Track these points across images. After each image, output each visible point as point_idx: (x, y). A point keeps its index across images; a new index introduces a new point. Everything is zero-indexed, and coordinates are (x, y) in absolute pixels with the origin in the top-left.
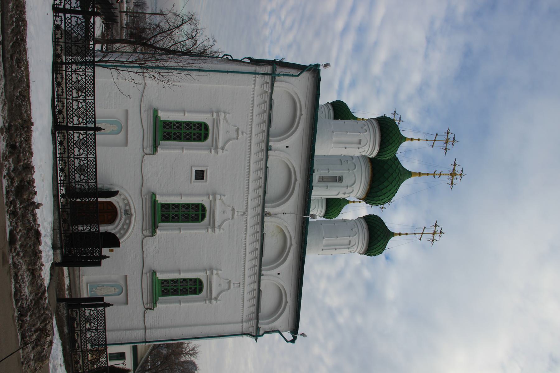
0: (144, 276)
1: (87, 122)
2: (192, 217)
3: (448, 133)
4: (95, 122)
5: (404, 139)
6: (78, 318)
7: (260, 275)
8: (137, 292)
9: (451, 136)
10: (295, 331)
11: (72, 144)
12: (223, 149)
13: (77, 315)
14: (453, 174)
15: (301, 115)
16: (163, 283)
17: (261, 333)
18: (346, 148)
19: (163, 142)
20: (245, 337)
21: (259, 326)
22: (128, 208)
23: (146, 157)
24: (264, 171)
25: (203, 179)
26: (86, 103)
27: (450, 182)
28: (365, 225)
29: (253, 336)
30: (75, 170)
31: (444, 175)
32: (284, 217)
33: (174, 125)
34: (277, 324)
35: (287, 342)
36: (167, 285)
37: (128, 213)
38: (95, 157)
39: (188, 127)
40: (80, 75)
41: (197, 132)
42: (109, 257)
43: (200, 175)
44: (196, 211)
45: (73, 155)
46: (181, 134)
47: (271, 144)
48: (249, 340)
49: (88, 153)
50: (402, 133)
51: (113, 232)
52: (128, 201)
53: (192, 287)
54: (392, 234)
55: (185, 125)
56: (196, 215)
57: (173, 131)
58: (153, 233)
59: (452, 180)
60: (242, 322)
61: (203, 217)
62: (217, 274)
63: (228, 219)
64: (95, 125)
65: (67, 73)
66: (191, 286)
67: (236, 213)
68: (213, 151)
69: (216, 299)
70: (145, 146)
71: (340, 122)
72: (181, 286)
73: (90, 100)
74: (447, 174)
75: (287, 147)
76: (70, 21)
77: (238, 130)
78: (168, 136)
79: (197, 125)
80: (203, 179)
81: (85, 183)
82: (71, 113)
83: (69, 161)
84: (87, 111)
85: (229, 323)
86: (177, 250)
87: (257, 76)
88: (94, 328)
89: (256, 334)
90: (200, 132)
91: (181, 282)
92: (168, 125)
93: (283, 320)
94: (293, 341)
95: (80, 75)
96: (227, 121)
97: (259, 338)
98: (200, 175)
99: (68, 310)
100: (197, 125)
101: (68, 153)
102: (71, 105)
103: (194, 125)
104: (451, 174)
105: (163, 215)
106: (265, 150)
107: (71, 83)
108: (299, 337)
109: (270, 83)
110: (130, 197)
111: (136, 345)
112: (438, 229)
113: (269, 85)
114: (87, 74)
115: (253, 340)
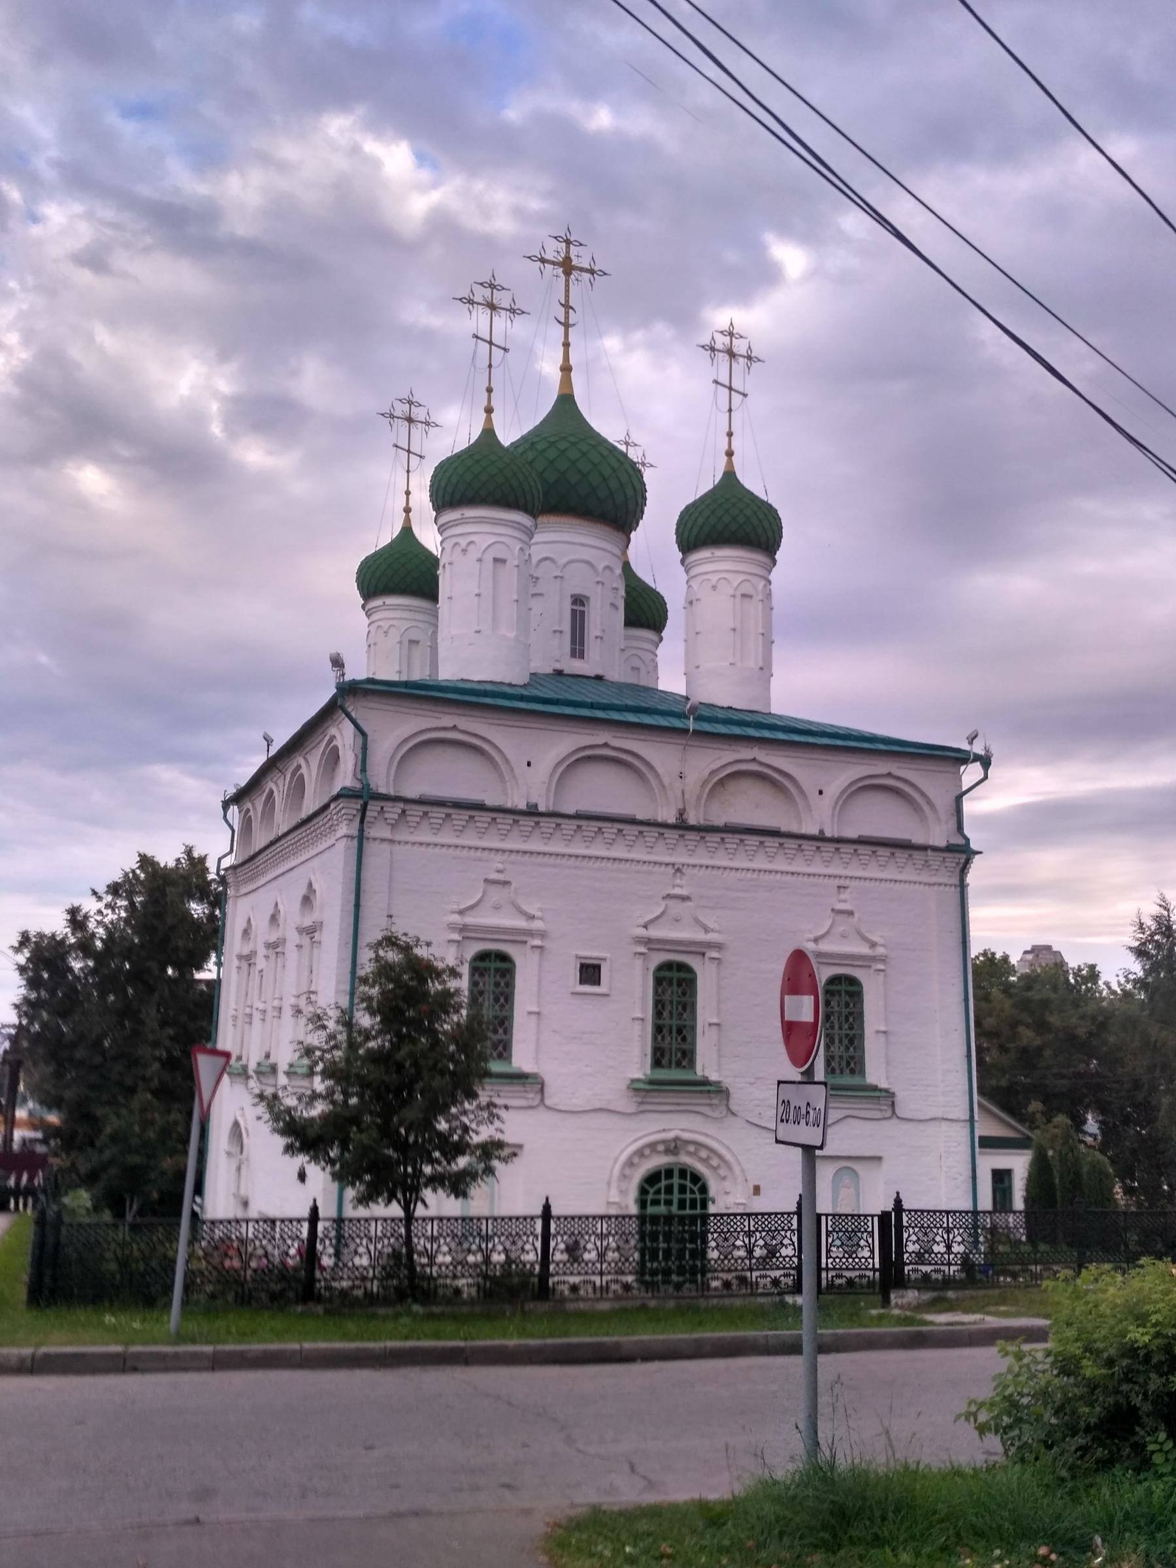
2: (684, 994)
4: (299, 1221)
6: (848, 1274)
10: (960, 758)
13: (841, 1276)
16: (833, 1071)
19: (514, 1059)
20: (970, 879)
21: (942, 843)
22: (661, 1148)
23: (548, 1102)
24: (583, 823)
28: (705, 554)
32: (681, 773)
35: (986, 777)
36: (837, 1059)
37: (674, 1146)
42: (898, 1193)
43: (590, 973)
54: (730, 476)
56: (679, 985)
58: (888, 1097)
64: (538, 1217)
66: (843, 1004)
72: (840, 1028)
78: (500, 1048)
80: (598, 967)
81: (750, 1237)
83: (834, 1269)
85: (283, 874)
87: (366, 834)
88: (747, 1241)
90: (492, 972)
91: (832, 1027)
97: (974, 846)
99: (906, 1288)
105: (679, 1064)
106: (536, 819)
109: (383, 804)
111: (977, 1140)
113: (388, 806)
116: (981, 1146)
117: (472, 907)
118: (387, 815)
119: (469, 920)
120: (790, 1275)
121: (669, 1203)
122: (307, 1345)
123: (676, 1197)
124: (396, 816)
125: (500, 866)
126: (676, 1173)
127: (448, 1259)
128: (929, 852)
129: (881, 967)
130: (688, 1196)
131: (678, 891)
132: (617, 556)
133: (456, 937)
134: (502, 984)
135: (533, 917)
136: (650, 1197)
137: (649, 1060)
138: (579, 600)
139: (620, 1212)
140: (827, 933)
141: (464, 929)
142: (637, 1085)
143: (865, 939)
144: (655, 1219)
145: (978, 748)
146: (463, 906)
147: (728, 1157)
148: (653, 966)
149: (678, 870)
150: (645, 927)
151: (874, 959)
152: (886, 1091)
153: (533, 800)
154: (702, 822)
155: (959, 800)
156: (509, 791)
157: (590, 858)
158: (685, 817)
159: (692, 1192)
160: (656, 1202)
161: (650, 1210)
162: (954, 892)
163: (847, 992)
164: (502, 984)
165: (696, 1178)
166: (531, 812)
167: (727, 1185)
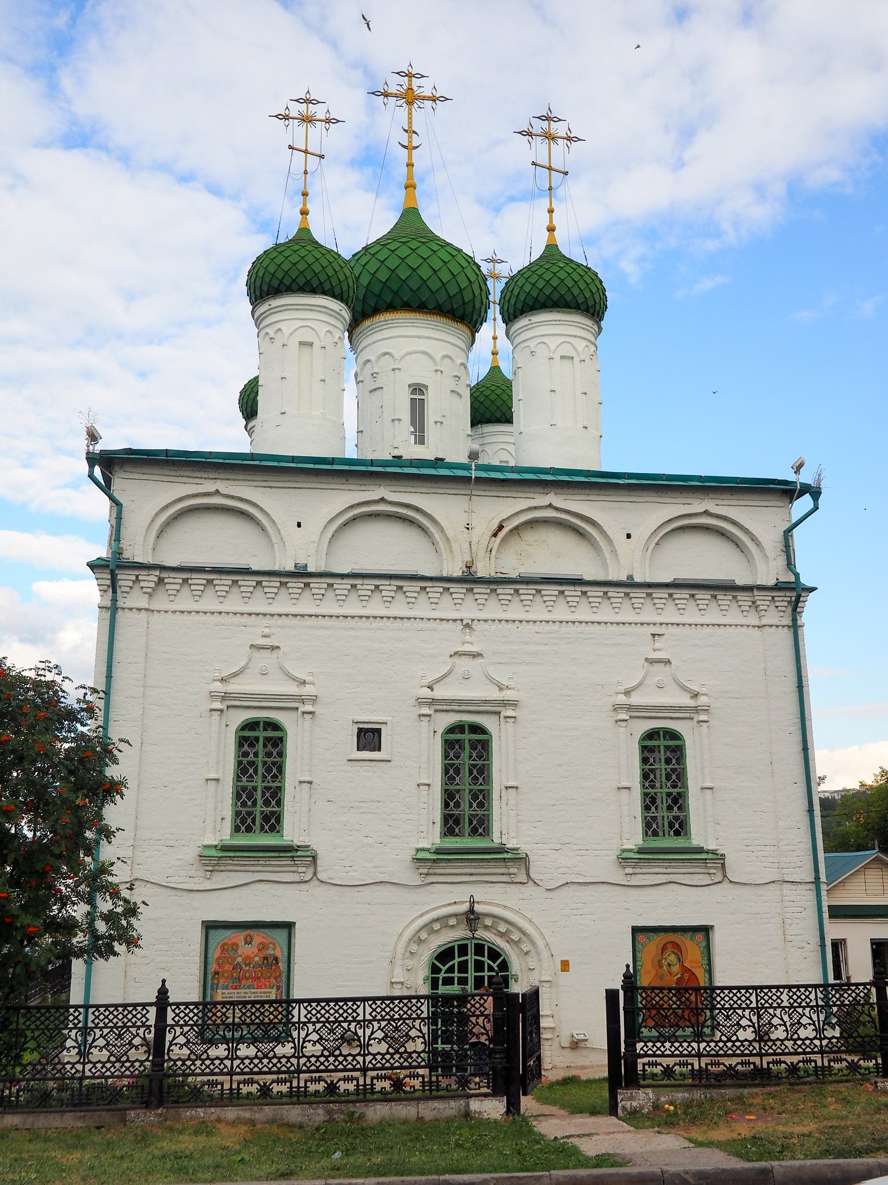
0: (635, 881)
1: (144, 1025)
3: (286, 118)
4: (144, 1005)
5: (552, 250)
7: (630, 584)
9: (296, 109)
10: (788, 492)
12: (695, 695)
13: (251, 1082)
14: (410, 98)
16: (655, 834)
17: (792, 579)
20: (806, 618)
21: (771, 582)
23: (320, 876)
24: (358, 582)
26: (177, 1024)
27: (428, 103)
28: (523, 322)
29: (798, 597)
30: (397, 1052)
31: (410, 123)
32: (465, 524)
33: (244, 804)
34: (771, 538)
35: (816, 508)
38: (364, 1000)
39: (251, 771)
41: (261, 749)
43: (369, 738)
44: (462, 747)
46: (267, 788)
48: (811, 606)
49: (354, 1020)
50: (536, 256)
52: (437, 920)
53: (663, 758)
57: (260, 808)
59: (424, 98)
61: (476, 729)
64: (151, 1004)
65: (88, 1074)
70: (295, 877)
71: (519, 410)
73: (364, 1012)
74: (410, 114)
76: (650, 1044)
78: (273, 821)
79: (246, 748)
80: (379, 731)
82: (198, 1063)
84: (115, 1026)
86: (566, 798)
87: (120, 604)
89: (793, 593)
92: (243, 821)
93: (761, 520)
94: (815, 493)
99: (639, 1087)
100: (246, 748)
101: (690, 1055)
102: (313, 1060)
103: (246, 754)
104: (410, 103)
105: (474, 832)
111: (825, 909)
112: (539, 126)
113: (143, 574)
114: (303, 1019)
115: (811, 599)
116: (831, 916)
117: (235, 675)
118: (142, 584)
119: (233, 687)
121: (463, 981)
123: (471, 974)
124: (152, 585)
125: (266, 631)
126: (471, 949)
128: (756, 593)
129: (703, 717)
130: (486, 974)
131: (467, 648)
132: (463, 350)
133: (217, 705)
134: (275, 754)
135: (304, 683)
136: (441, 975)
137: (438, 828)
138: (418, 389)
139: (406, 993)
140: (640, 684)
141: (225, 697)
142: (421, 855)
143: (684, 689)
144: (448, 999)
145: (806, 477)
146: (225, 674)
147: (530, 930)
148: (441, 729)
149: (467, 626)
150: (431, 688)
151: (696, 710)
152: (714, 852)
153: (301, 561)
154: (493, 574)
155: (788, 533)
156: (277, 554)
157: (368, 617)
158: (473, 569)
159: (491, 969)
160: (448, 981)
161: (442, 990)
162: (786, 635)
163: (667, 748)
164: (275, 754)
165: (494, 954)
166: (301, 573)
167: (532, 962)
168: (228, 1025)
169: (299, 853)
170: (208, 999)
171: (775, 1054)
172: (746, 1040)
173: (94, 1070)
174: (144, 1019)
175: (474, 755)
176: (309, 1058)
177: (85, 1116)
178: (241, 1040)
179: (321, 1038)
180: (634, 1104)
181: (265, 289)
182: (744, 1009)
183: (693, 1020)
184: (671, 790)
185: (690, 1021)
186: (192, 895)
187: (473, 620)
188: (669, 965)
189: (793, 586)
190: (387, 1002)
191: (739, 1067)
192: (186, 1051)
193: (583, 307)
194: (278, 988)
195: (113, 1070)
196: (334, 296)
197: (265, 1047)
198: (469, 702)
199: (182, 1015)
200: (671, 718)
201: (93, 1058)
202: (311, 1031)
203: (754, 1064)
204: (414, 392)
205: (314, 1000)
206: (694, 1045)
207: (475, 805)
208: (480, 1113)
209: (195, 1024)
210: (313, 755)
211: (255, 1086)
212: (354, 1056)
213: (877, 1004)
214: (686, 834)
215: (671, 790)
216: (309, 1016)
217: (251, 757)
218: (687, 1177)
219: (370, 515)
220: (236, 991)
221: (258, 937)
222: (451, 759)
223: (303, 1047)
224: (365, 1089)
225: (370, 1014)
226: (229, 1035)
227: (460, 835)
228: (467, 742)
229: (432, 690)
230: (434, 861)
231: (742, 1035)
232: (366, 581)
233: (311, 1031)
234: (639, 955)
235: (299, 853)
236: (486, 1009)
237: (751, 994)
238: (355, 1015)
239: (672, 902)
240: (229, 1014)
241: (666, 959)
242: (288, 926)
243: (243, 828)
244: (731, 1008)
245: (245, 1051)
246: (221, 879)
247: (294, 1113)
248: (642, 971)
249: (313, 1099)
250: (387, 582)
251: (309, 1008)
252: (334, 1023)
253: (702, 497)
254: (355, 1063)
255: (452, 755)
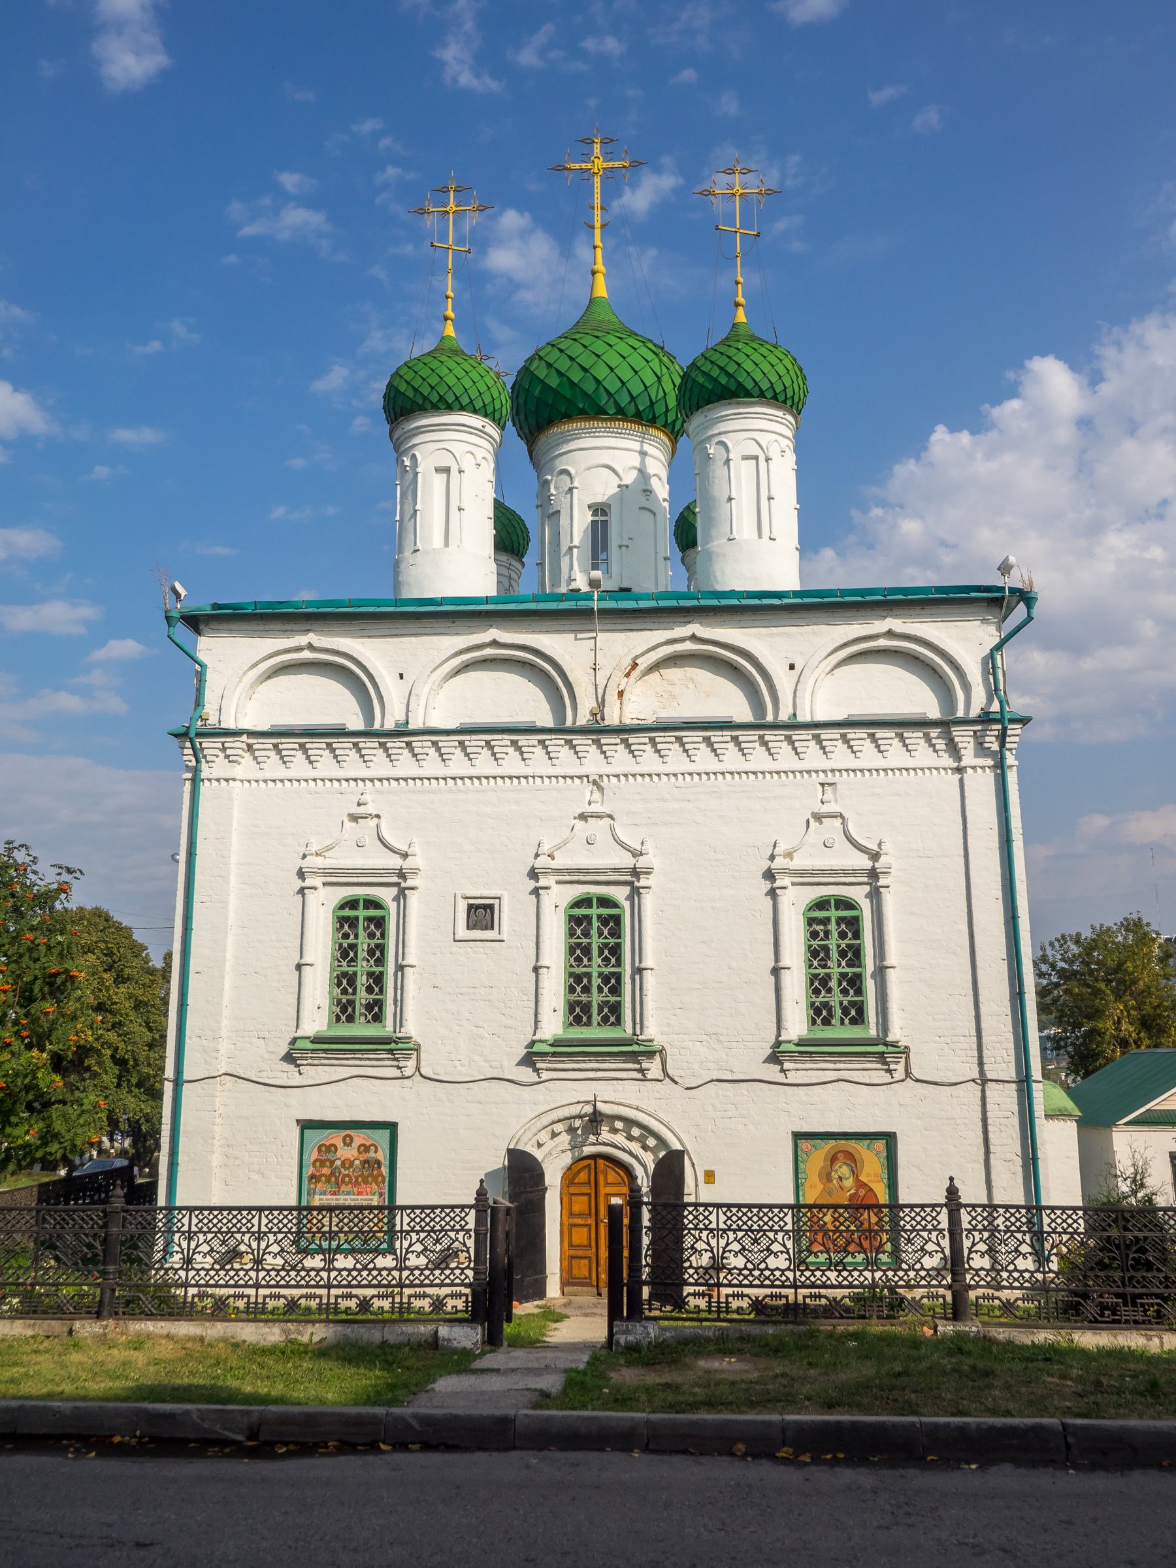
0: (793, 1077)
8: (846, 1101)
11: (365, 1273)
13: (350, 1296)
15: (310, 647)
18: (730, 499)
25: (491, 907)
35: (1030, 618)
40: (410, 1245)
41: (364, 930)
44: (590, 923)
45: (324, 1274)
47: (390, 725)
51: (651, 1167)
55: (345, 963)
60: (960, 770)
62: (789, 855)
63: (612, 829)
64: (470, 1207)
67: (595, 808)
68: (410, 883)
69: (875, 857)
70: (397, 1073)
75: (401, 676)
77: (354, 818)
80: (491, 907)
84: (433, 1230)
86: (715, 980)
88: (254, 1245)
92: (344, 1010)
95: (410, 1245)
96: (329, 848)
98: (482, 915)
107: (751, 1270)
108: (1014, 580)
110: (533, 1117)
114: (722, 1226)
120: (461, 1295)
122: (790, 1417)
127: (422, 1261)
168: (324, 1233)
169: (400, 1046)
170: (304, 1203)
171: (813, 1286)
172: (777, 1269)
173: (339, 1278)
174: (463, 1223)
175: (606, 932)
176: (268, 1271)
177: (34, 1325)
178: (338, 1250)
179: (744, 1248)
180: (630, 1338)
181: (398, 411)
182: (776, 1232)
183: (866, 1244)
184: (847, 970)
185: (861, 1245)
186: (736, 1085)
187: (601, 776)
188: (840, 1178)
189: (998, 716)
190: (745, 1210)
191: (925, 1301)
192: (279, 1261)
193: (769, 395)
194: (381, 1195)
195: (307, 1279)
196: (475, 411)
197: (365, 1258)
198: (597, 871)
199: (734, 1218)
200: (845, 884)
201: (337, 1265)
202: (271, 1241)
203: (787, 1297)
204: (595, 513)
205: (418, 1207)
206: (867, 1274)
207: (606, 990)
208: (449, 1340)
209: (290, 1232)
210: (425, 932)
211: (355, 1300)
212: (247, 1271)
213: (475, 1230)
214: (863, 1022)
215: (847, 970)
216: (412, 1224)
217: (351, 940)
218: (415, 1424)
219: (485, 661)
220: (334, 1197)
221: (360, 1137)
222: (579, 937)
223: (405, 1259)
224: (328, 1309)
225: (725, 1223)
226: (325, 1245)
227: (589, 1024)
228: (595, 919)
229: (553, 859)
230: (554, 1054)
231: (772, 1262)
232: (474, 737)
233: (271, 1241)
234: (801, 1165)
235: (400, 1046)
236: (939, 1223)
237: (786, 1215)
238: (249, 1225)
239: (846, 1101)
240: (326, 1221)
241: (836, 1171)
242: (392, 1127)
243: (343, 1018)
244: (914, 1230)
245: (342, 1262)
246: (312, 1074)
247: (249, 1333)
248: (807, 1185)
249: (735, 1316)
250: (499, 737)
251: (729, 1214)
252: (227, 1233)
253: (885, 613)
254: (463, 1277)
255: (579, 932)
